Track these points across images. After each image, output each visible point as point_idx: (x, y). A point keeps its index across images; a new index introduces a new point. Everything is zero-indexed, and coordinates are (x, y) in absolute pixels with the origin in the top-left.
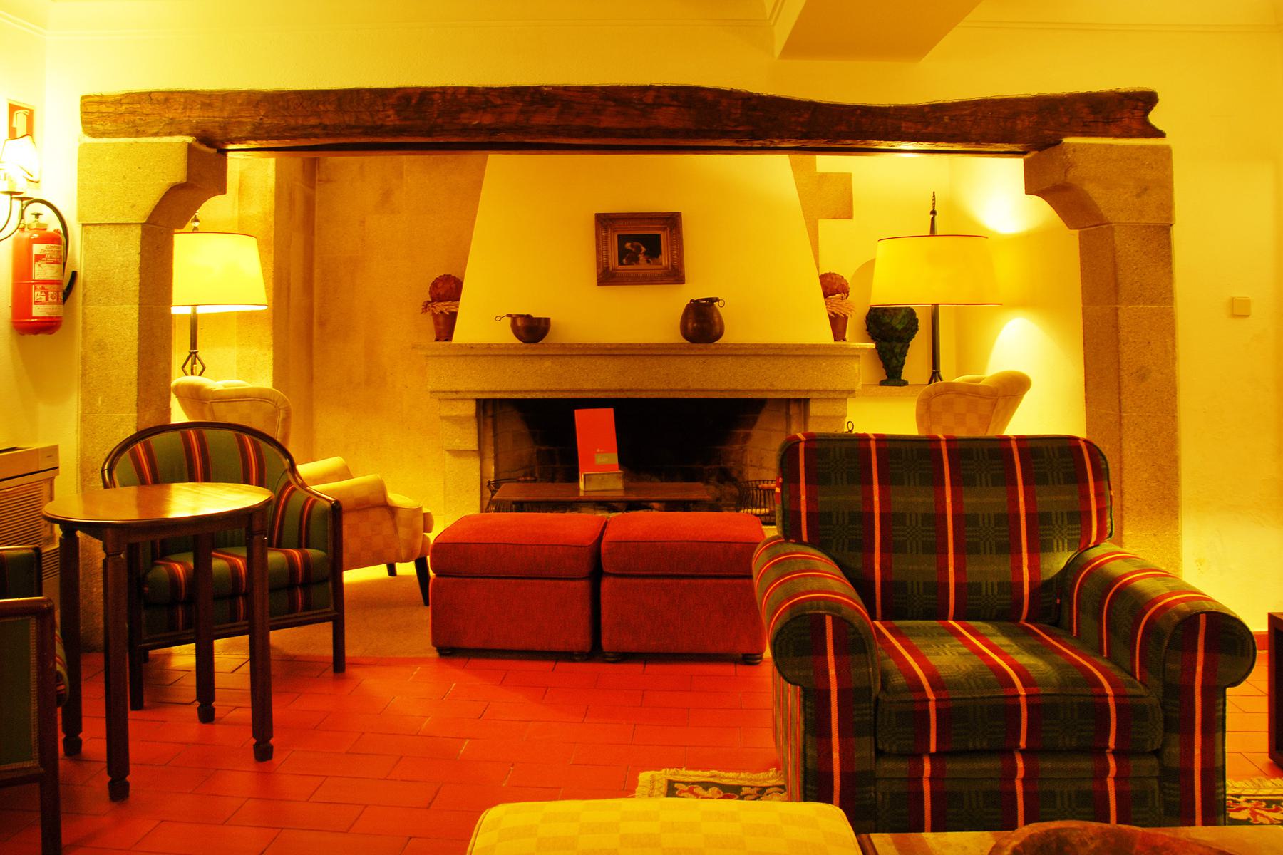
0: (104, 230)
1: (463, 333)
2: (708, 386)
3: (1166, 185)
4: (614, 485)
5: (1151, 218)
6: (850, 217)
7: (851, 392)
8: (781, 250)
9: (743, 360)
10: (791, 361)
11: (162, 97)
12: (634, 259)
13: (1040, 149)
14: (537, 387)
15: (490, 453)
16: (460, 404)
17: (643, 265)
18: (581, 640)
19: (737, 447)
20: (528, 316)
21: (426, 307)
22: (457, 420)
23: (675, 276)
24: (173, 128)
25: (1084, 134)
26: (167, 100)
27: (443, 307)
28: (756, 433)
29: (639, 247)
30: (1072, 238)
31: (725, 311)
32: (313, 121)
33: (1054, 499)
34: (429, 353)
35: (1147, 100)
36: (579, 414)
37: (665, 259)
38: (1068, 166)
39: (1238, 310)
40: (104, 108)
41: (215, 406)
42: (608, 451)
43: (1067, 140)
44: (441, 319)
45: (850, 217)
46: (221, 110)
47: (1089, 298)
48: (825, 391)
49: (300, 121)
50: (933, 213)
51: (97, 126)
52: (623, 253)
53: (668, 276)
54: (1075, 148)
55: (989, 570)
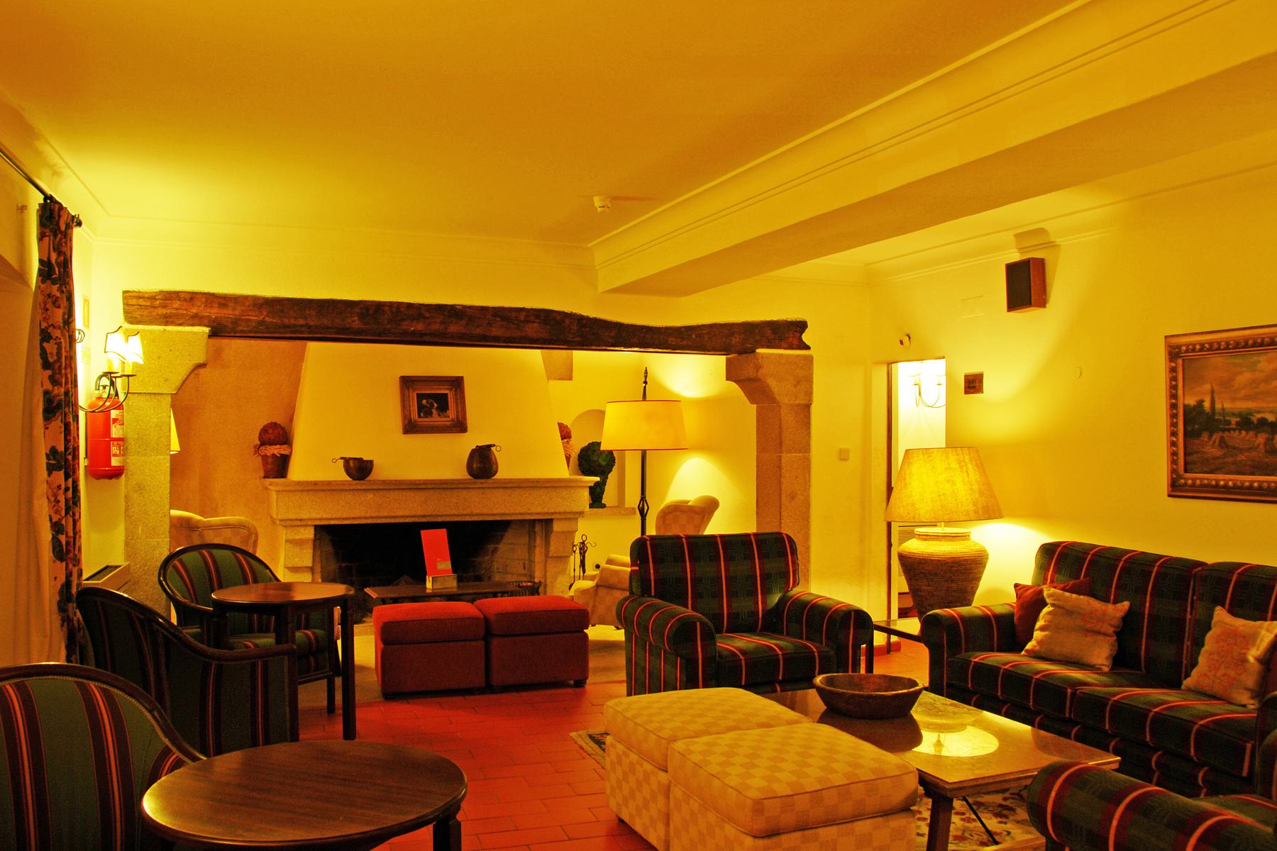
0: (141, 398)
1: (298, 471)
2: (485, 511)
3: (809, 380)
4: (451, 584)
5: (802, 401)
6: (570, 378)
7: (581, 513)
8: (529, 408)
9: (509, 491)
10: (542, 491)
11: (188, 297)
12: (428, 413)
13: (740, 353)
14: (363, 514)
15: (318, 569)
16: (302, 529)
17: (436, 419)
18: (480, 681)
19: (487, 558)
20: (360, 459)
21: (257, 449)
22: (299, 543)
23: (460, 426)
24: (196, 320)
25: (768, 347)
26: (191, 299)
27: (276, 450)
28: (503, 547)
29: (433, 405)
30: (750, 410)
31: (499, 455)
32: (301, 322)
33: (773, 566)
34: (281, 488)
35: (802, 326)
36: (425, 534)
37: (452, 413)
38: (758, 367)
39: (843, 456)
40: (141, 302)
41: (206, 532)
42: (444, 560)
43: (759, 351)
44: (270, 460)
45: (570, 378)
46: (234, 309)
47: (761, 448)
48: (565, 513)
49: (292, 321)
50: (645, 382)
51: (137, 314)
52: (421, 408)
53: (455, 426)
54: (763, 356)
55: (743, 605)
